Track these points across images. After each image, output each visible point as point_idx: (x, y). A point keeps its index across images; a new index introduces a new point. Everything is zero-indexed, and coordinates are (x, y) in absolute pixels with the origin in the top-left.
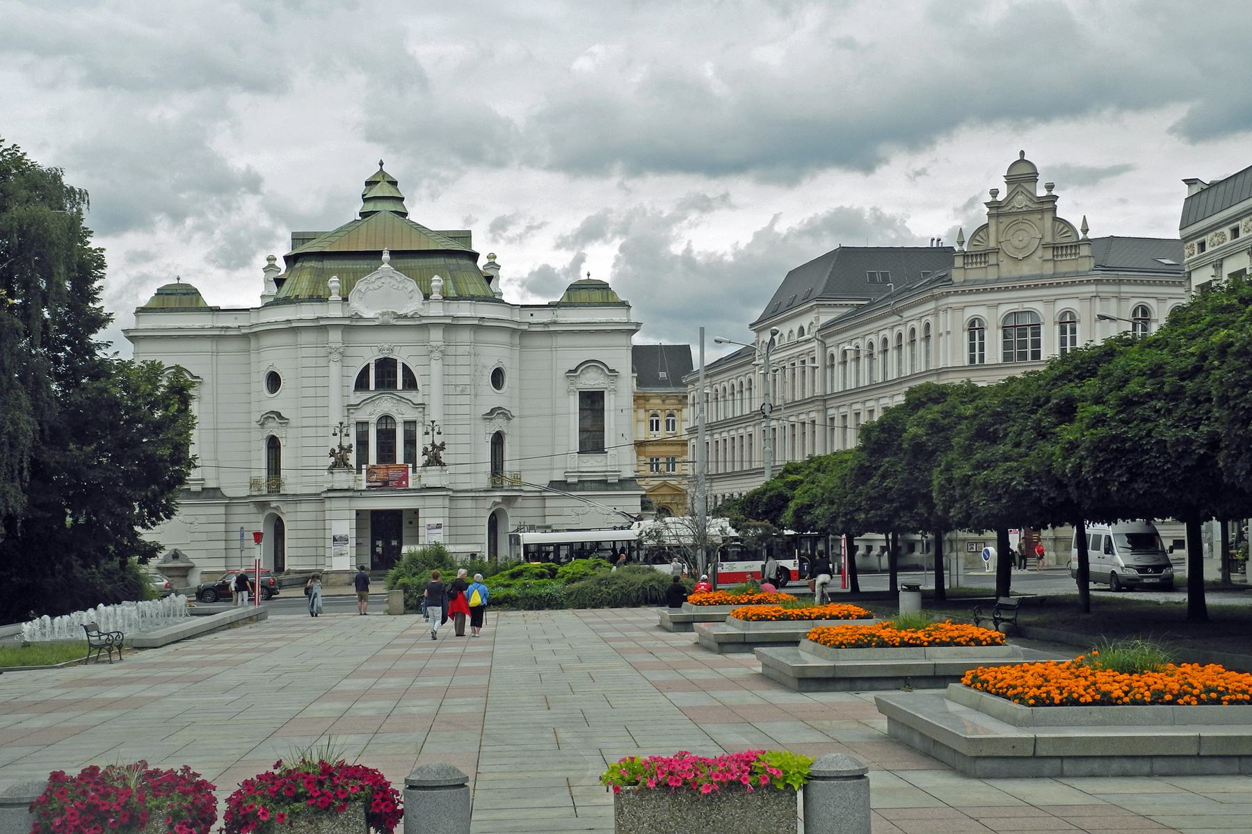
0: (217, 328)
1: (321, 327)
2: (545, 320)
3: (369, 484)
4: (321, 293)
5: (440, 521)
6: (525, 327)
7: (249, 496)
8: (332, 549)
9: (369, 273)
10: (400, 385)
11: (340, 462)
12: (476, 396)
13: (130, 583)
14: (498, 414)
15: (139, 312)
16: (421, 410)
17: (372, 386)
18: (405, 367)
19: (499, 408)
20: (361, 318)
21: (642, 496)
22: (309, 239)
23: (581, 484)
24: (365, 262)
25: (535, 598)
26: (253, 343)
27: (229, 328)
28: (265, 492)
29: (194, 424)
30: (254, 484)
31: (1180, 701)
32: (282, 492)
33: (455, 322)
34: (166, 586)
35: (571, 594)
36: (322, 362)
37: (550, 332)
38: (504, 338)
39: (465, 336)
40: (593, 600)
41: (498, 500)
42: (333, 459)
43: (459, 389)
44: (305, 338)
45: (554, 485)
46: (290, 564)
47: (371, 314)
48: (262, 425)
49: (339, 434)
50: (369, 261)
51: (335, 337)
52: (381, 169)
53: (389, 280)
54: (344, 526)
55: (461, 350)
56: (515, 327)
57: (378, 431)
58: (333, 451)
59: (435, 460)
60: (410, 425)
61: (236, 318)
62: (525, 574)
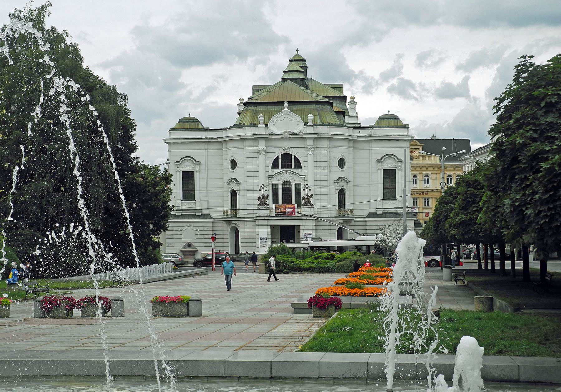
0: (207, 138)
1: (255, 139)
2: (366, 135)
3: (276, 214)
4: (256, 122)
5: (310, 231)
6: (355, 138)
7: (222, 218)
8: (259, 244)
9: (279, 112)
10: (293, 166)
11: (263, 202)
12: (330, 171)
13: (152, 258)
14: (341, 180)
15: (171, 130)
16: (304, 178)
17: (280, 167)
18: (295, 157)
19: (342, 177)
20: (274, 134)
21: (415, 220)
22: (261, 89)
23: (385, 215)
24: (277, 107)
25: (322, 268)
26: (224, 146)
27: (213, 138)
28: (230, 216)
29: (171, 193)
30: (225, 212)
31: (354, 295)
32: (238, 216)
33: (319, 136)
34: (180, 259)
35: (339, 267)
36: (256, 155)
37: (368, 140)
38: (345, 143)
39: (325, 143)
40: (348, 269)
41: (342, 222)
42: (259, 202)
43: (322, 168)
44: (248, 143)
45: (371, 215)
46: (242, 250)
47: (279, 133)
48: (228, 184)
49: (262, 190)
50: (279, 107)
51: (262, 143)
52: (297, 54)
53: (287, 116)
54: (265, 233)
55: (323, 150)
56: (351, 138)
57: (283, 188)
58: (260, 198)
59: (308, 203)
60: (298, 186)
61: (216, 134)
62: (320, 258)
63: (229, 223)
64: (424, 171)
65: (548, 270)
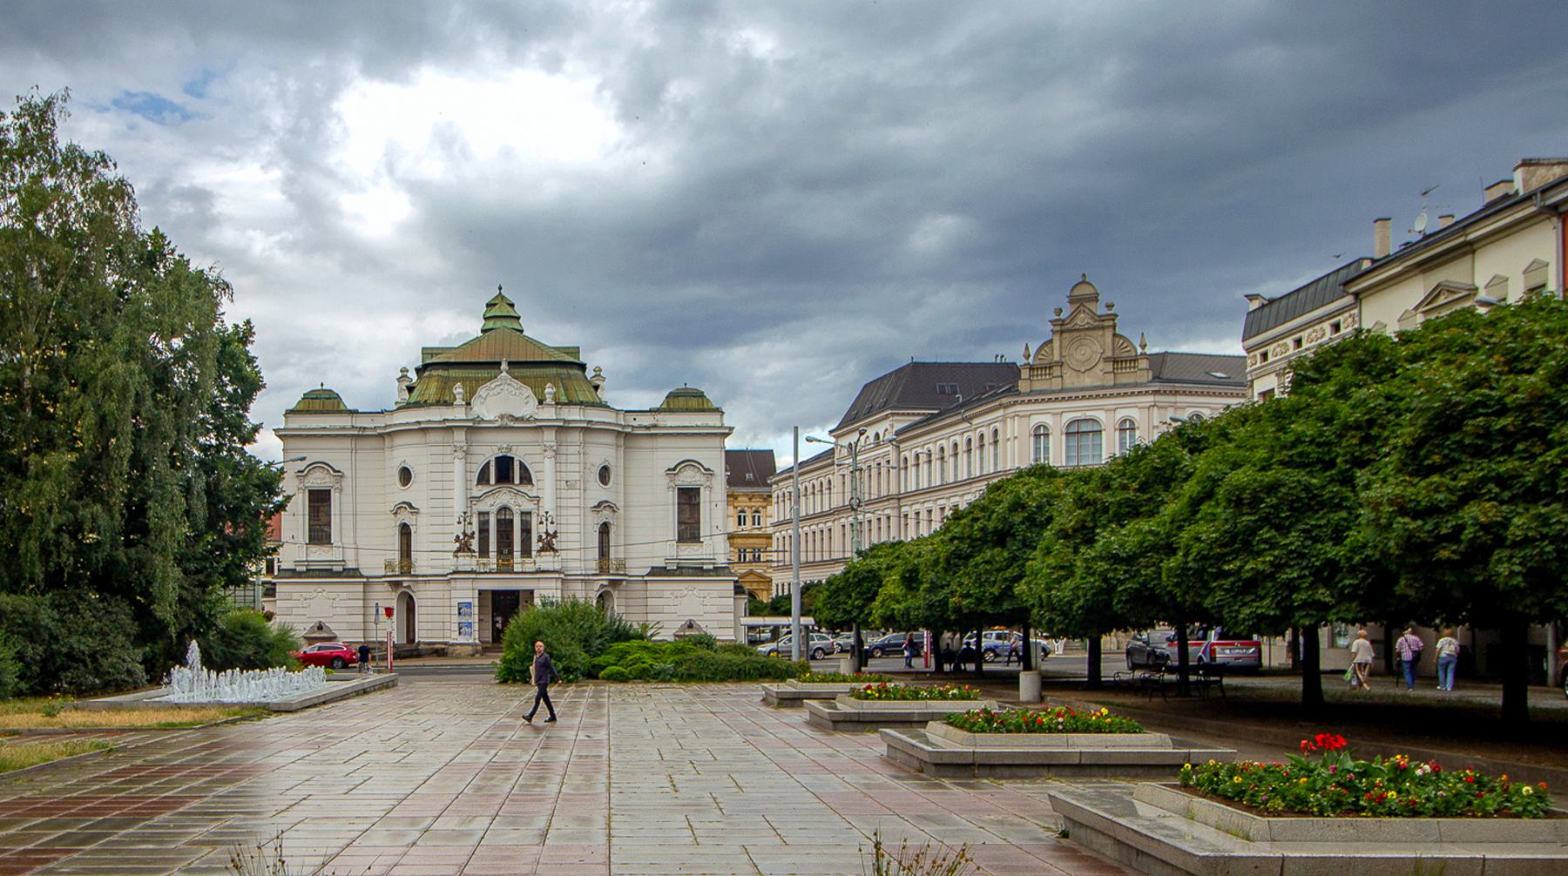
11: (464, 548)
59: (548, 547)
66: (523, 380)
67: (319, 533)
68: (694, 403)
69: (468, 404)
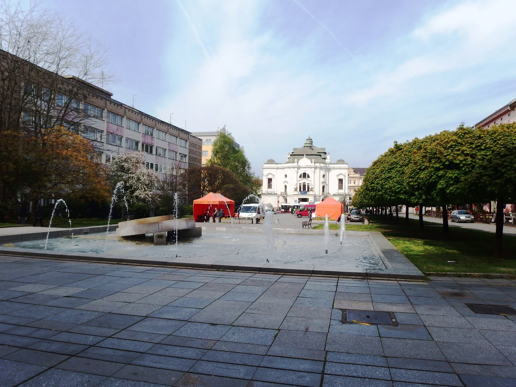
11: (296, 190)
44: (291, 169)
59: (312, 190)
63: (284, 196)
64: (354, 179)
65: (409, 218)
66: (309, 158)
67: (270, 186)
68: (342, 162)
69: (298, 163)
